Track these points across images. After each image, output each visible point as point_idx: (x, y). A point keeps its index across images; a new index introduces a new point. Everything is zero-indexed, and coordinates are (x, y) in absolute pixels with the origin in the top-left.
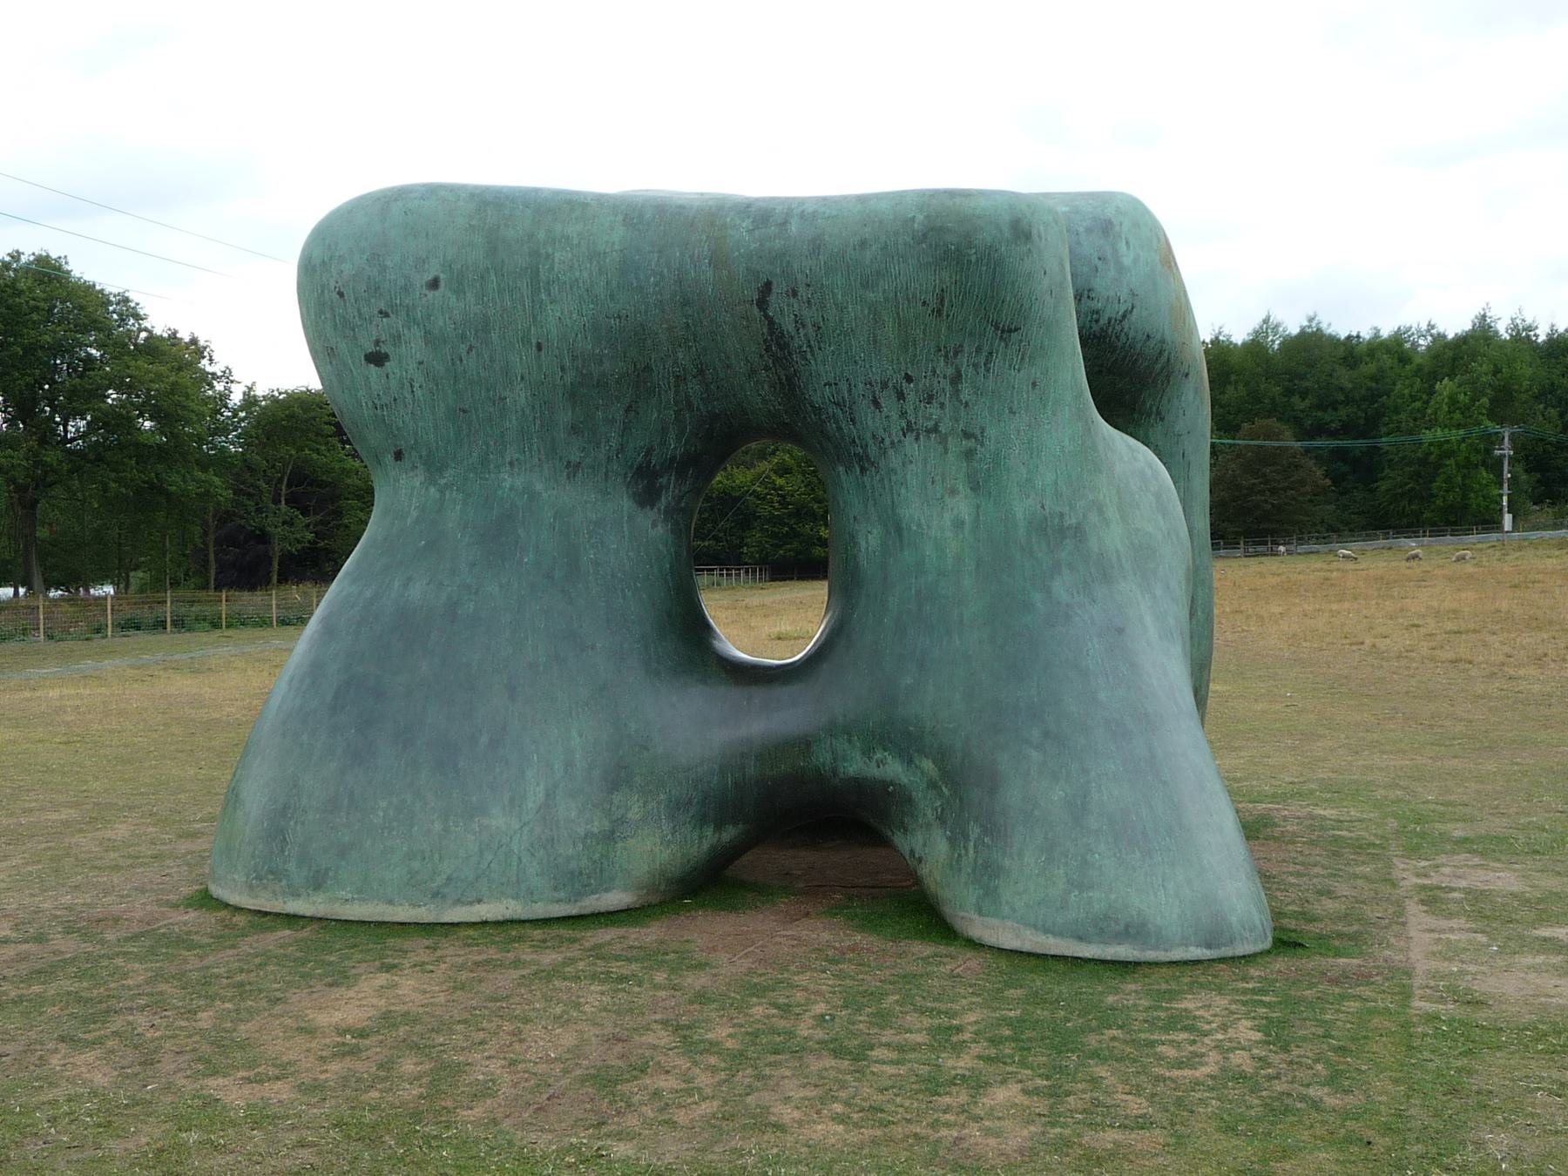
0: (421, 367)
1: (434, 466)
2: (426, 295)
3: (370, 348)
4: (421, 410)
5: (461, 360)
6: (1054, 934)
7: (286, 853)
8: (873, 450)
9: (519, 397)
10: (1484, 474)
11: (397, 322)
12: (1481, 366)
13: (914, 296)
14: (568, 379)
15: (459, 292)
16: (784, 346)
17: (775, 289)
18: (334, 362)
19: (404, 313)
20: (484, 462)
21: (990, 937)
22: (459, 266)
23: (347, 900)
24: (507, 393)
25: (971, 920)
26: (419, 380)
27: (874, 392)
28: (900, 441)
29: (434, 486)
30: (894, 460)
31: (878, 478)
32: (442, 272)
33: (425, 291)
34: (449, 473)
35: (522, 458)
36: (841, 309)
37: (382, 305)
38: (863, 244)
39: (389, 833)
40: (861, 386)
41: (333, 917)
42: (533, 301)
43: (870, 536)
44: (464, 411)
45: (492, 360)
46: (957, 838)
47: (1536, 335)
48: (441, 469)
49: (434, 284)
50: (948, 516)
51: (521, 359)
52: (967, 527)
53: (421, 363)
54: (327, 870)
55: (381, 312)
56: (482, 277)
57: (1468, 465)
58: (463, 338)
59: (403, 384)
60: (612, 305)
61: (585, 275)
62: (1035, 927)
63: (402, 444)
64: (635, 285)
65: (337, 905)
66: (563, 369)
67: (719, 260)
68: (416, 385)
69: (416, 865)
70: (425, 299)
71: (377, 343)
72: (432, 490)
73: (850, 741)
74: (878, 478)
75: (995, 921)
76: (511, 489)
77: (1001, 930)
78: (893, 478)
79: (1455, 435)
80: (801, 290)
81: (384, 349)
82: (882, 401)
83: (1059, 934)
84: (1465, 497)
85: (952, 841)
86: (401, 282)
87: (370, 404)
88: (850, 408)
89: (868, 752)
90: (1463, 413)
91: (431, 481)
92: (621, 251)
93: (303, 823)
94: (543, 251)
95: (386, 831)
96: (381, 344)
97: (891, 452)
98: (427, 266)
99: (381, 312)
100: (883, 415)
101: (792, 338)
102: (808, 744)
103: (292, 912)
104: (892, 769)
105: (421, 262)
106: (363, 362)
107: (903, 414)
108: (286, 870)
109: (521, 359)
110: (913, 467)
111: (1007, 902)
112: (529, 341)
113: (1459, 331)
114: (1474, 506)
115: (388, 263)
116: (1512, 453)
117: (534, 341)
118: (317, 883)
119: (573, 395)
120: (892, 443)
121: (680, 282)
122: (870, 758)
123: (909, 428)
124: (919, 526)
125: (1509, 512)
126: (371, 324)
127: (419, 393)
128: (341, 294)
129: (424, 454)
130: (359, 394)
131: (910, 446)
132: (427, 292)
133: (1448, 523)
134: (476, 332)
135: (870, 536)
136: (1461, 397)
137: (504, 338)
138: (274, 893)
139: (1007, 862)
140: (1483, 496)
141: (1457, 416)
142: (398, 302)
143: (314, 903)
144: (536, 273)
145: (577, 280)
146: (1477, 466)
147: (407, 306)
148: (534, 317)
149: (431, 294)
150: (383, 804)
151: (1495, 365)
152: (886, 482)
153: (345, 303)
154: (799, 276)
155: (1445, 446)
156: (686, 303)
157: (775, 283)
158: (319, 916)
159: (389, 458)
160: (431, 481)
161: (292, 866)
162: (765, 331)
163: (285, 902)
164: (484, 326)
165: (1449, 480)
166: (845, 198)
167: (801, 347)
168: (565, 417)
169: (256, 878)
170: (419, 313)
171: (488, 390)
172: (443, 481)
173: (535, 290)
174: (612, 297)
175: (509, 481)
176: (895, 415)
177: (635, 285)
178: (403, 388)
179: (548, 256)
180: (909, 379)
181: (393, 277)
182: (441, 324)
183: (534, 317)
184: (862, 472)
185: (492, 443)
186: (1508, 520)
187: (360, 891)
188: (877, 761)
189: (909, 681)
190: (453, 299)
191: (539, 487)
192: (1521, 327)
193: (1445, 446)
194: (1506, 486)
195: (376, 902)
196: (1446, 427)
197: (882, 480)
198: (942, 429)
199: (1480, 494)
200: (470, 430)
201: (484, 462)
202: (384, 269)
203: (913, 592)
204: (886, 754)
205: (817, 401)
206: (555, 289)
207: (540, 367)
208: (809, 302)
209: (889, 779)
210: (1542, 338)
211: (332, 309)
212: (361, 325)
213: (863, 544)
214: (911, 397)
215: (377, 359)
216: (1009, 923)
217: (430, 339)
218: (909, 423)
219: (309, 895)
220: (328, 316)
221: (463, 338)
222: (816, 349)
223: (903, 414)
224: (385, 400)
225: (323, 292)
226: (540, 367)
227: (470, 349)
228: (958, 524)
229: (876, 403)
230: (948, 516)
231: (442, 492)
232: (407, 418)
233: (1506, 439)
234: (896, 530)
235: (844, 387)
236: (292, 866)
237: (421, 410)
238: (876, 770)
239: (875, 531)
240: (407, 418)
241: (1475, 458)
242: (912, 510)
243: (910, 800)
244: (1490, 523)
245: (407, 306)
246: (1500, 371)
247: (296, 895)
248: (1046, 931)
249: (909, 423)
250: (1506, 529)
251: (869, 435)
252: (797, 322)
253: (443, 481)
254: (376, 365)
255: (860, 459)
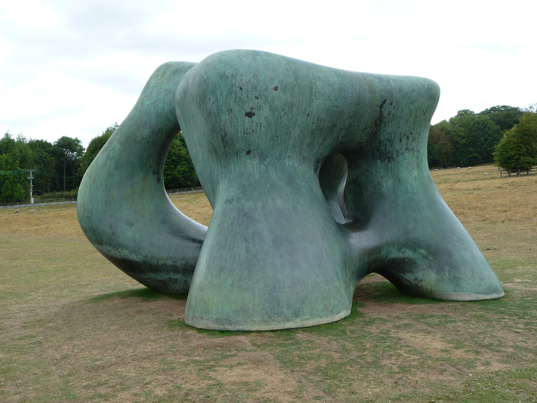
0: (266, 119)
1: (263, 157)
2: (273, 92)
3: (248, 110)
4: (262, 136)
5: (281, 118)
6: (480, 294)
7: (281, 305)
8: (395, 155)
9: (296, 132)
10: (19, 185)
11: (261, 101)
12: (16, 149)
13: (422, 108)
14: (314, 127)
15: (284, 92)
16: (381, 121)
17: (387, 102)
18: (230, 115)
19: (264, 98)
20: (280, 156)
21: (460, 298)
22: (285, 83)
23: (308, 319)
24: (292, 131)
25: (452, 294)
26: (264, 123)
27: (401, 137)
28: (404, 153)
29: (263, 164)
30: (401, 158)
31: (394, 164)
32: (279, 85)
33: (273, 91)
34: (268, 160)
35: (292, 155)
36: (403, 110)
37: (257, 95)
38: (413, 91)
39: (315, 292)
40: (398, 135)
41: (304, 327)
42: (310, 99)
43: (388, 182)
44: (277, 137)
45: (292, 118)
46: (439, 270)
47: (26, 141)
48: (265, 159)
49: (276, 89)
50: (413, 176)
51: (301, 119)
52: (417, 179)
53: (266, 118)
54: (299, 309)
55: (256, 97)
56: (293, 88)
57: (14, 183)
58: (283, 110)
59: (258, 125)
60: (335, 103)
61: (328, 91)
62: (475, 293)
63: (251, 148)
64: (344, 96)
65: (305, 321)
66: (313, 123)
67: (372, 91)
68: (262, 126)
69: (325, 302)
70: (272, 94)
71: (252, 109)
72: (262, 166)
73: (393, 247)
74: (394, 164)
75: (462, 293)
76: (289, 166)
77: (465, 295)
78: (399, 164)
79: (9, 173)
80: (394, 104)
81: (254, 111)
82: (403, 140)
83: (481, 293)
84: (13, 193)
85: (438, 273)
86: (264, 86)
87: (242, 132)
88: (392, 142)
89: (399, 250)
90: (11, 165)
91: (261, 162)
92: (339, 84)
93: (285, 293)
94: (313, 81)
95: (314, 291)
96: (253, 109)
97: (400, 156)
98: (274, 82)
99: (256, 97)
100: (402, 144)
101: (385, 118)
102: (380, 249)
103: (288, 328)
104: (409, 254)
105: (272, 80)
106: (244, 116)
107: (407, 144)
108: (283, 312)
109: (301, 119)
110: (405, 161)
111: (465, 287)
112: (305, 113)
113: (61, 137)
114: (16, 196)
115: (260, 79)
116: (33, 178)
117: (307, 113)
118: (296, 315)
119: (313, 133)
120: (401, 153)
121: (359, 97)
122: (400, 251)
123: (407, 149)
124: (406, 179)
125: (33, 197)
126: (251, 101)
127: (263, 129)
128: (241, 89)
129: (259, 152)
130: (238, 128)
131: (406, 155)
132: (273, 91)
133: (7, 202)
134: (288, 108)
135: (388, 182)
136: (10, 160)
137: (298, 111)
138: (279, 322)
139: (461, 276)
140: (19, 193)
141: (9, 166)
142: (263, 93)
143: (296, 322)
144: (311, 89)
145: (325, 93)
146: (16, 183)
147: (266, 96)
148: (309, 104)
149: (275, 92)
150: (310, 281)
151: (20, 150)
152: (396, 165)
153: (242, 92)
154: (394, 99)
155: (5, 176)
156: (359, 104)
157: (387, 101)
158: (298, 327)
159: (244, 154)
160: (261, 162)
161: (284, 310)
162: (378, 116)
163: (284, 325)
164: (292, 106)
165: (7, 187)
166: (372, 75)
167: (386, 121)
168: (307, 141)
169: (268, 317)
170: (270, 99)
171: (287, 129)
172: (266, 163)
173: (311, 95)
174: (336, 100)
175: (288, 163)
176: (405, 144)
177: (344, 96)
178: (257, 127)
179: (315, 83)
180: (411, 133)
181: (262, 84)
182: (277, 103)
183: (309, 104)
184: (388, 162)
185: (284, 149)
186: (32, 200)
187: (311, 315)
188: (402, 252)
189: (412, 226)
190: (282, 94)
191: (296, 165)
192: (21, 138)
193: (5, 176)
194: (31, 189)
195: (316, 318)
196: (5, 170)
197: (395, 165)
198: (414, 150)
199: (18, 192)
200: (277, 144)
201: (280, 156)
202: (258, 81)
203: (406, 199)
204: (406, 249)
205: (382, 139)
206: (317, 95)
207: (306, 122)
208: (394, 107)
209: (406, 257)
210: (28, 142)
211: (236, 94)
212: (247, 101)
213: (385, 185)
214: (410, 139)
215: (250, 115)
216: (467, 293)
217: (272, 109)
218: (407, 147)
219: (293, 320)
220: (233, 96)
221: (283, 110)
222: (390, 122)
223: (407, 144)
224: (249, 131)
225: (232, 87)
226: (306, 122)
227: (285, 114)
228: (415, 178)
229: (401, 141)
230: (413, 176)
231: (266, 167)
232: (256, 138)
233: (31, 174)
234: (398, 180)
235: (393, 135)
236: (284, 310)
237: (262, 136)
238: (401, 255)
239: (390, 181)
240: (256, 138)
241: (16, 180)
242: (404, 174)
243: (415, 263)
244: (23, 200)
245: (266, 96)
246: (22, 152)
247: (288, 320)
248: (478, 293)
249: (407, 147)
250: (32, 203)
251: (395, 151)
252: (388, 113)
253: (266, 163)
254: (249, 117)
255: (389, 158)
